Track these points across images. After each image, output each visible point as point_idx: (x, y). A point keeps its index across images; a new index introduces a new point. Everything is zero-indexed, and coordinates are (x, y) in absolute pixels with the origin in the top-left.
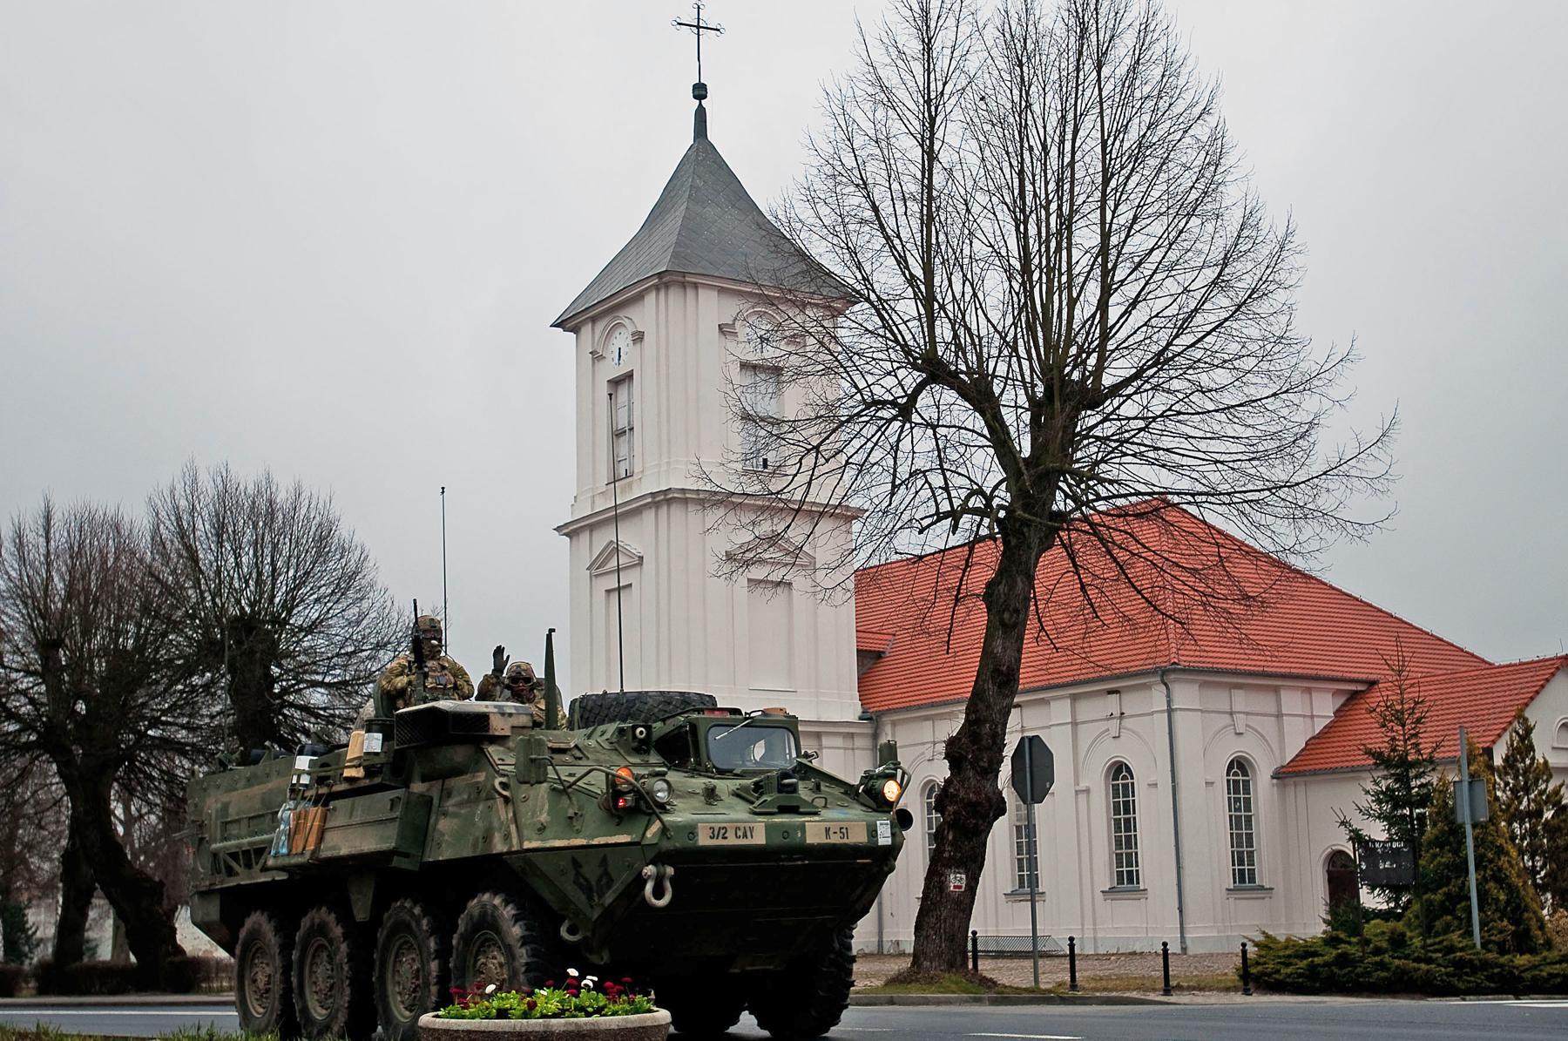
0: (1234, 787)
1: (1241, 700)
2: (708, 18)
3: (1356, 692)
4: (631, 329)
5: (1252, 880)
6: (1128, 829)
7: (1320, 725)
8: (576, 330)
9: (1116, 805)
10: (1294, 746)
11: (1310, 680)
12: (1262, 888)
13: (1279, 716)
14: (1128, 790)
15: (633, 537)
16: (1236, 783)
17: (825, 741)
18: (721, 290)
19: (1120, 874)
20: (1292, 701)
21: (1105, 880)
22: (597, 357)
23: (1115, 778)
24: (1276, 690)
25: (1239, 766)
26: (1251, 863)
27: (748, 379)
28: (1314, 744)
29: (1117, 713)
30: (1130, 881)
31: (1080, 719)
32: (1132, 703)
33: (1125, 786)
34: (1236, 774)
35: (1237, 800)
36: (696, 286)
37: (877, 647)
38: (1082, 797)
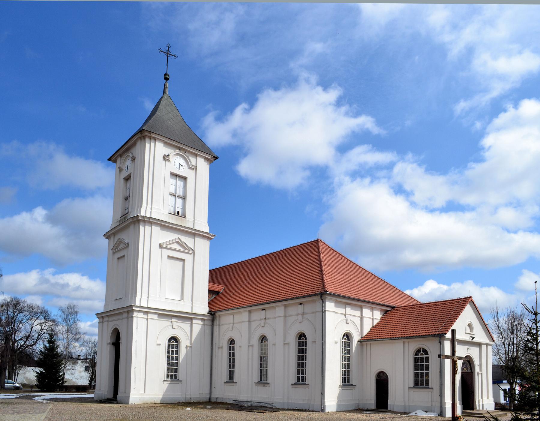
0: (344, 344)
1: (349, 310)
2: (172, 51)
3: (388, 311)
4: (131, 156)
5: (348, 382)
6: (303, 360)
7: (376, 322)
8: (115, 162)
9: (299, 350)
10: (367, 330)
11: (373, 304)
12: (352, 385)
13: (147, 319)
14: (304, 344)
15: (124, 236)
16: (345, 342)
17: (194, 321)
18: (165, 143)
19: (298, 378)
20: (367, 312)
21: (294, 380)
22: (121, 170)
23: (230, 344)
24: (361, 308)
25: (347, 336)
26: (348, 375)
27: (173, 181)
28: (374, 328)
29: (263, 318)
30: (302, 380)
31: (267, 317)
32: (269, 313)
33: (265, 345)
34: (345, 339)
35: (345, 350)
36: (155, 139)
37: (218, 290)
38: (220, 350)
